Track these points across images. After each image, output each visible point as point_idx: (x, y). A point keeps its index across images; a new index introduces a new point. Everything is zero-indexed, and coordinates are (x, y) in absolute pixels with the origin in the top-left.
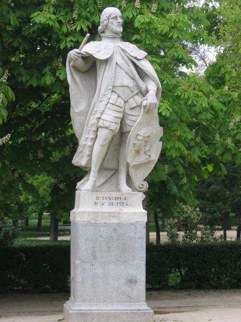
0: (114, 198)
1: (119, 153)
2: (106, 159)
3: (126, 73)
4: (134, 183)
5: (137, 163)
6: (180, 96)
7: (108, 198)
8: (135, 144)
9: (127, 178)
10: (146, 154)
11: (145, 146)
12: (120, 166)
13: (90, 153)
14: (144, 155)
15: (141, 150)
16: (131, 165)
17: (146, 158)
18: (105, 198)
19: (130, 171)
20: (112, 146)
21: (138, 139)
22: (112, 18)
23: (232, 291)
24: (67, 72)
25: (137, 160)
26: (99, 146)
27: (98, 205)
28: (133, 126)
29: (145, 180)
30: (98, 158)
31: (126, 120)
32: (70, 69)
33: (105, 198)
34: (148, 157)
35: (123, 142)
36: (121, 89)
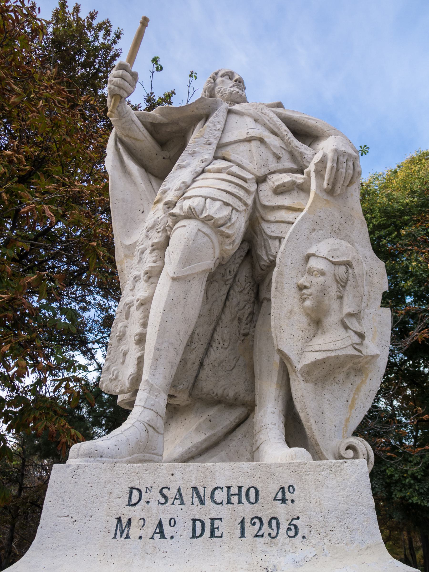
0: (220, 496)
1: (251, 350)
2: (206, 362)
3: (256, 121)
4: (292, 163)
5: (319, 356)
6: (393, 518)
7: (187, 495)
8: (301, 288)
9: (286, 425)
10: (346, 327)
11: (341, 298)
12: (258, 383)
13: (159, 263)
14: (342, 332)
15: (327, 313)
16: (299, 366)
17: (349, 342)
18: (172, 493)
19: (296, 395)
20: (227, 317)
21: (310, 272)
22: (222, 76)
23: (247, 297)
24: (107, 151)
25: (316, 348)
26: (170, 282)
27: (134, 531)
28: (284, 238)
29: (355, 434)
30: (213, 457)
31: (265, 226)
32: (117, 149)
33: (172, 493)
34: (356, 339)
35: (265, 304)
36: (244, 147)
